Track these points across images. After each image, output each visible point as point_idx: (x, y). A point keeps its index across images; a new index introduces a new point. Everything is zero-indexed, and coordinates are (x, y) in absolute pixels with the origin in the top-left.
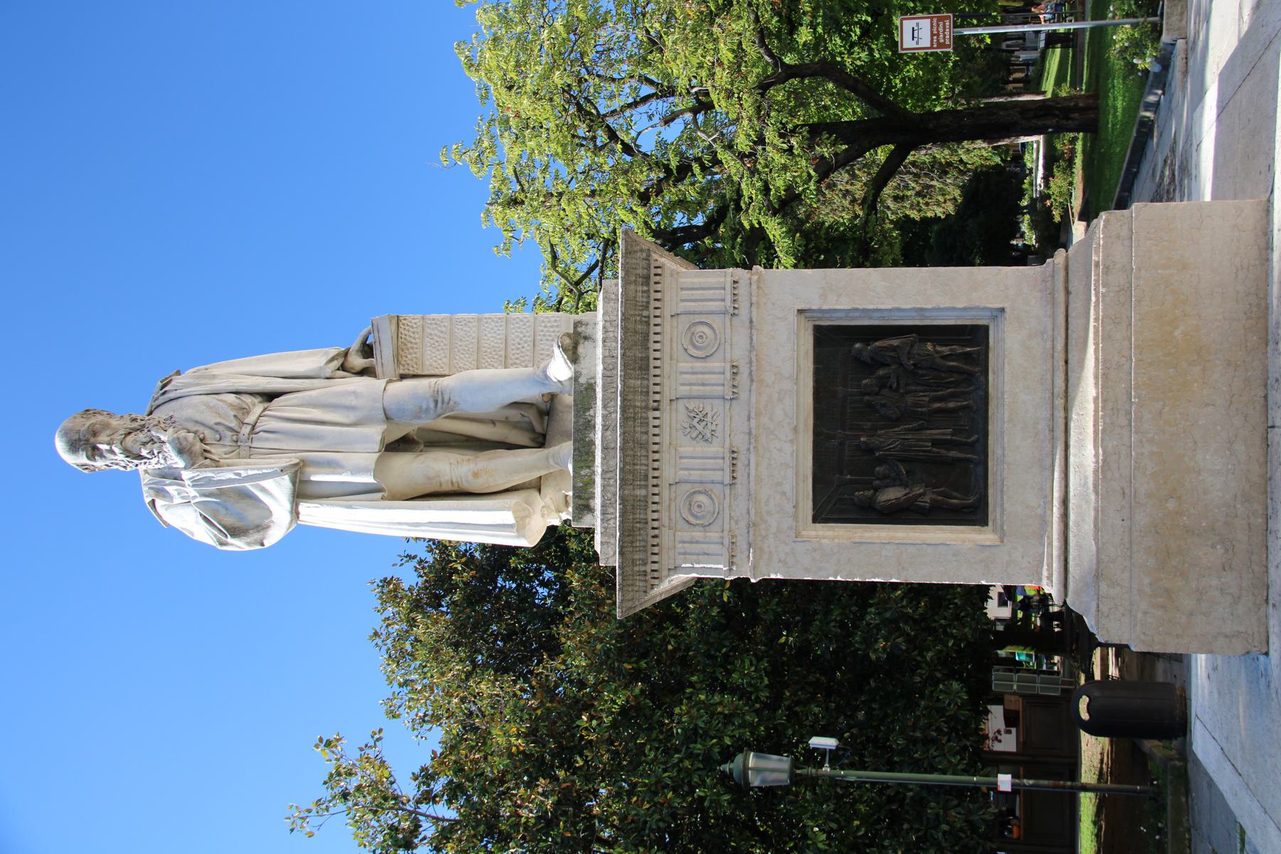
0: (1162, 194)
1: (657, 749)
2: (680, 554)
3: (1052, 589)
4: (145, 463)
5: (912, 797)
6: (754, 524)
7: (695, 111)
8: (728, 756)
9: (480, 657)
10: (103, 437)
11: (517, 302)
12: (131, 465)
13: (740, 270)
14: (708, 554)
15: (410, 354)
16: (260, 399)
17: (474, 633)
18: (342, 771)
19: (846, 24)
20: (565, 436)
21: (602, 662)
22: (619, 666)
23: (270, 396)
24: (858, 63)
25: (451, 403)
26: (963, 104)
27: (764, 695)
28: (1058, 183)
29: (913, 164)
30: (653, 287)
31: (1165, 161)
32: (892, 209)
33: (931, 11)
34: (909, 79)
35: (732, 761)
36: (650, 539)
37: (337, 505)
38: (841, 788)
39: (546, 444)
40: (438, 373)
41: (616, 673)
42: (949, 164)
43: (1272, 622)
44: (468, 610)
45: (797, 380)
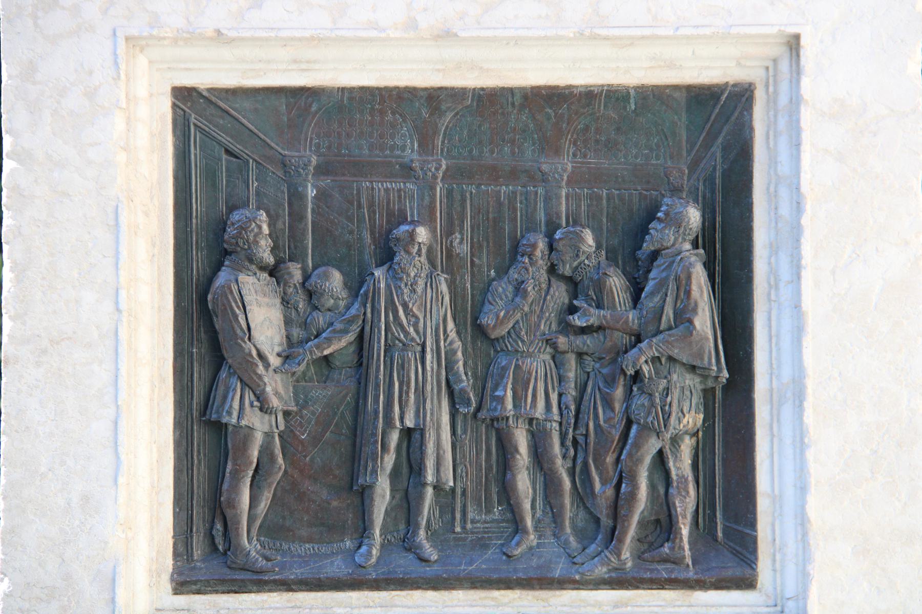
45: (595, 37)
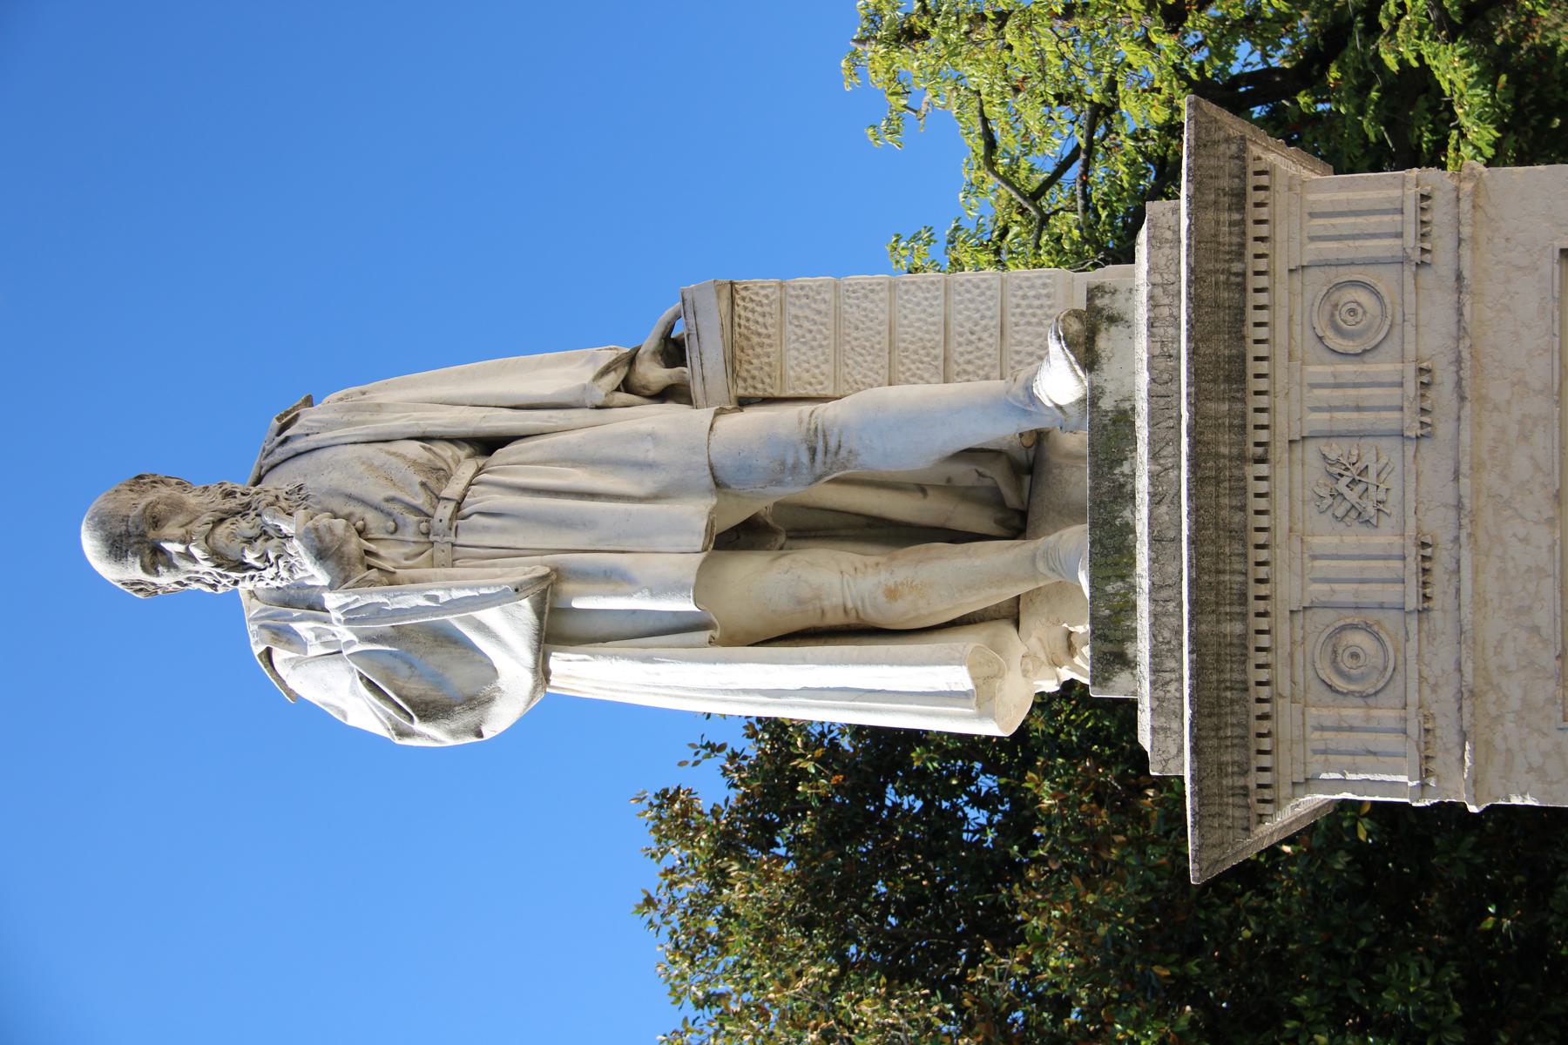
2: (1315, 752)
4: (252, 578)
6: (1472, 693)
9: (853, 949)
10: (172, 529)
11: (916, 238)
12: (224, 581)
14: (1375, 754)
15: (758, 357)
16: (468, 450)
17: (841, 899)
20: (1071, 514)
22: (1143, 972)
23: (487, 445)
25: (843, 453)
30: (1252, 213)
36: (1253, 722)
37: (623, 657)
39: (1029, 531)
40: (814, 394)
41: (1136, 986)
44: (830, 853)
45: (1560, 393)
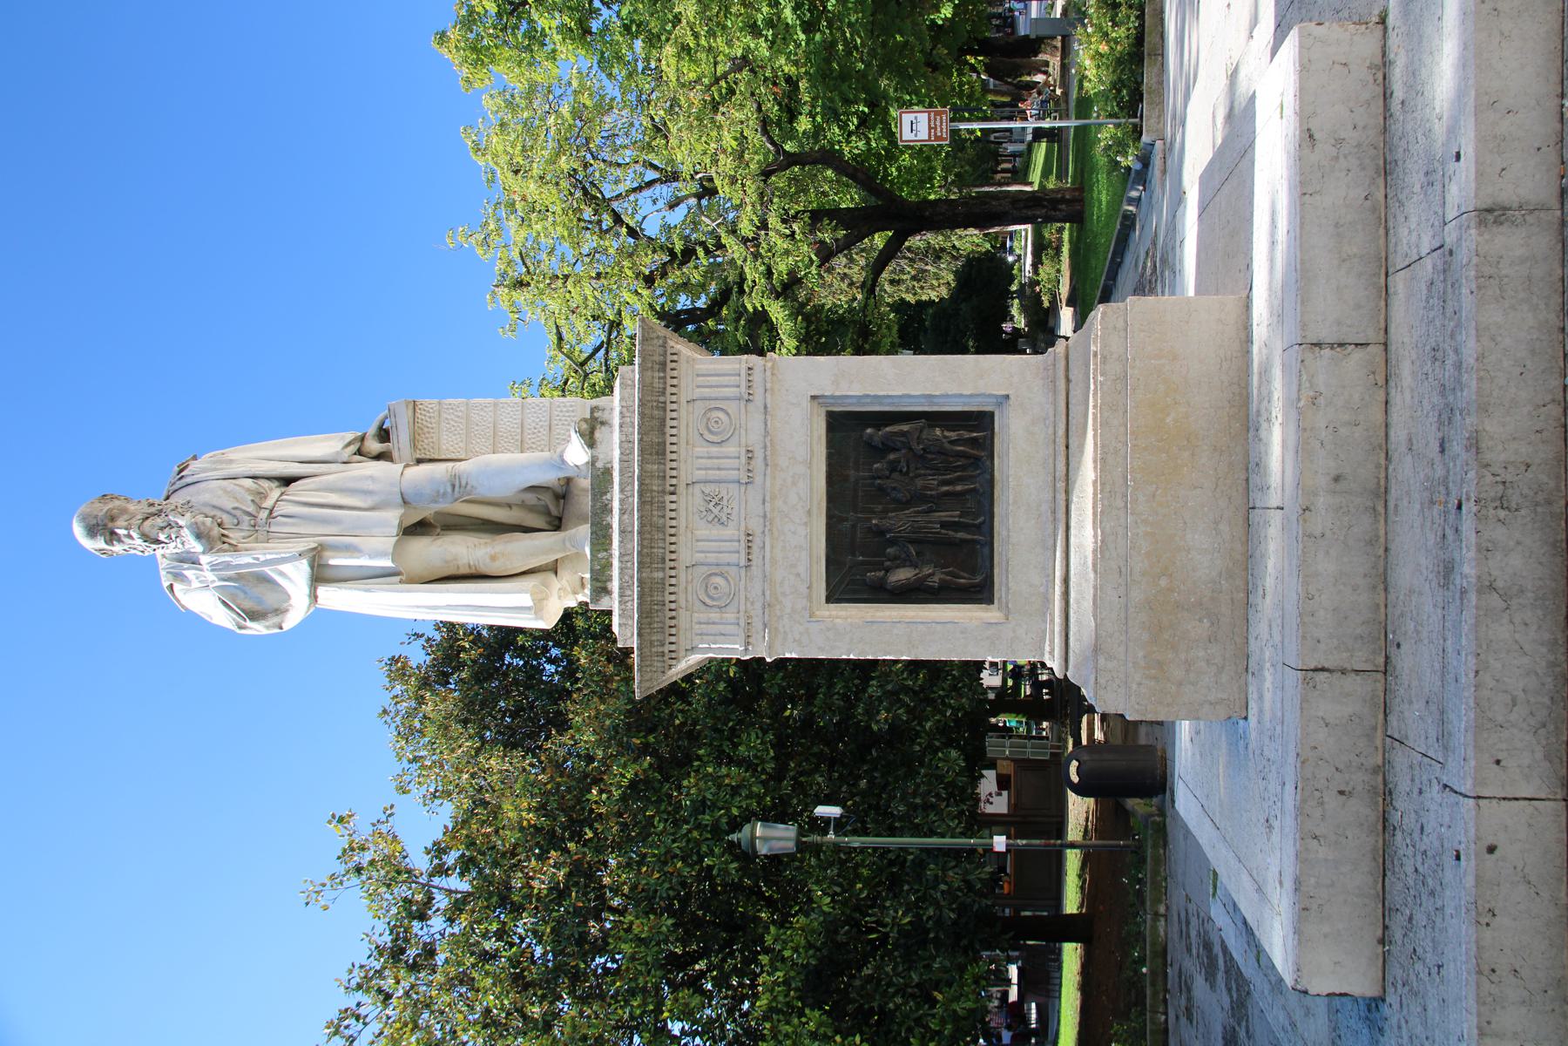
0: (1144, 287)
1: (666, 820)
2: (697, 635)
3: (1055, 664)
5: (913, 860)
7: (699, 197)
8: (735, 825)
9: (488, 734)
10: (121, 522)
11: (523, 383)
13: (754, 357)
15: (427, 438)
16: (277, 483)
17: (482, 709)
18: (355, 846)
19: (844, 114)
20: (582, 519)
21: (615, 737)
23: (287, 481)
24: (856, 152)
25: (469, 487)
26: (955, 193)
27: (770, 766)
28: (1046, 270)
29: (909, 249)
30: (670, 373)
31: (1147, 253)
32: (889, 293)
33: (926, 104)
34: (905, 168)
35: (740, 831)
38: (845, 854)
41: (624, 748)
42: (943, 250)
43: (1251, 689)
44: (476, 687)
